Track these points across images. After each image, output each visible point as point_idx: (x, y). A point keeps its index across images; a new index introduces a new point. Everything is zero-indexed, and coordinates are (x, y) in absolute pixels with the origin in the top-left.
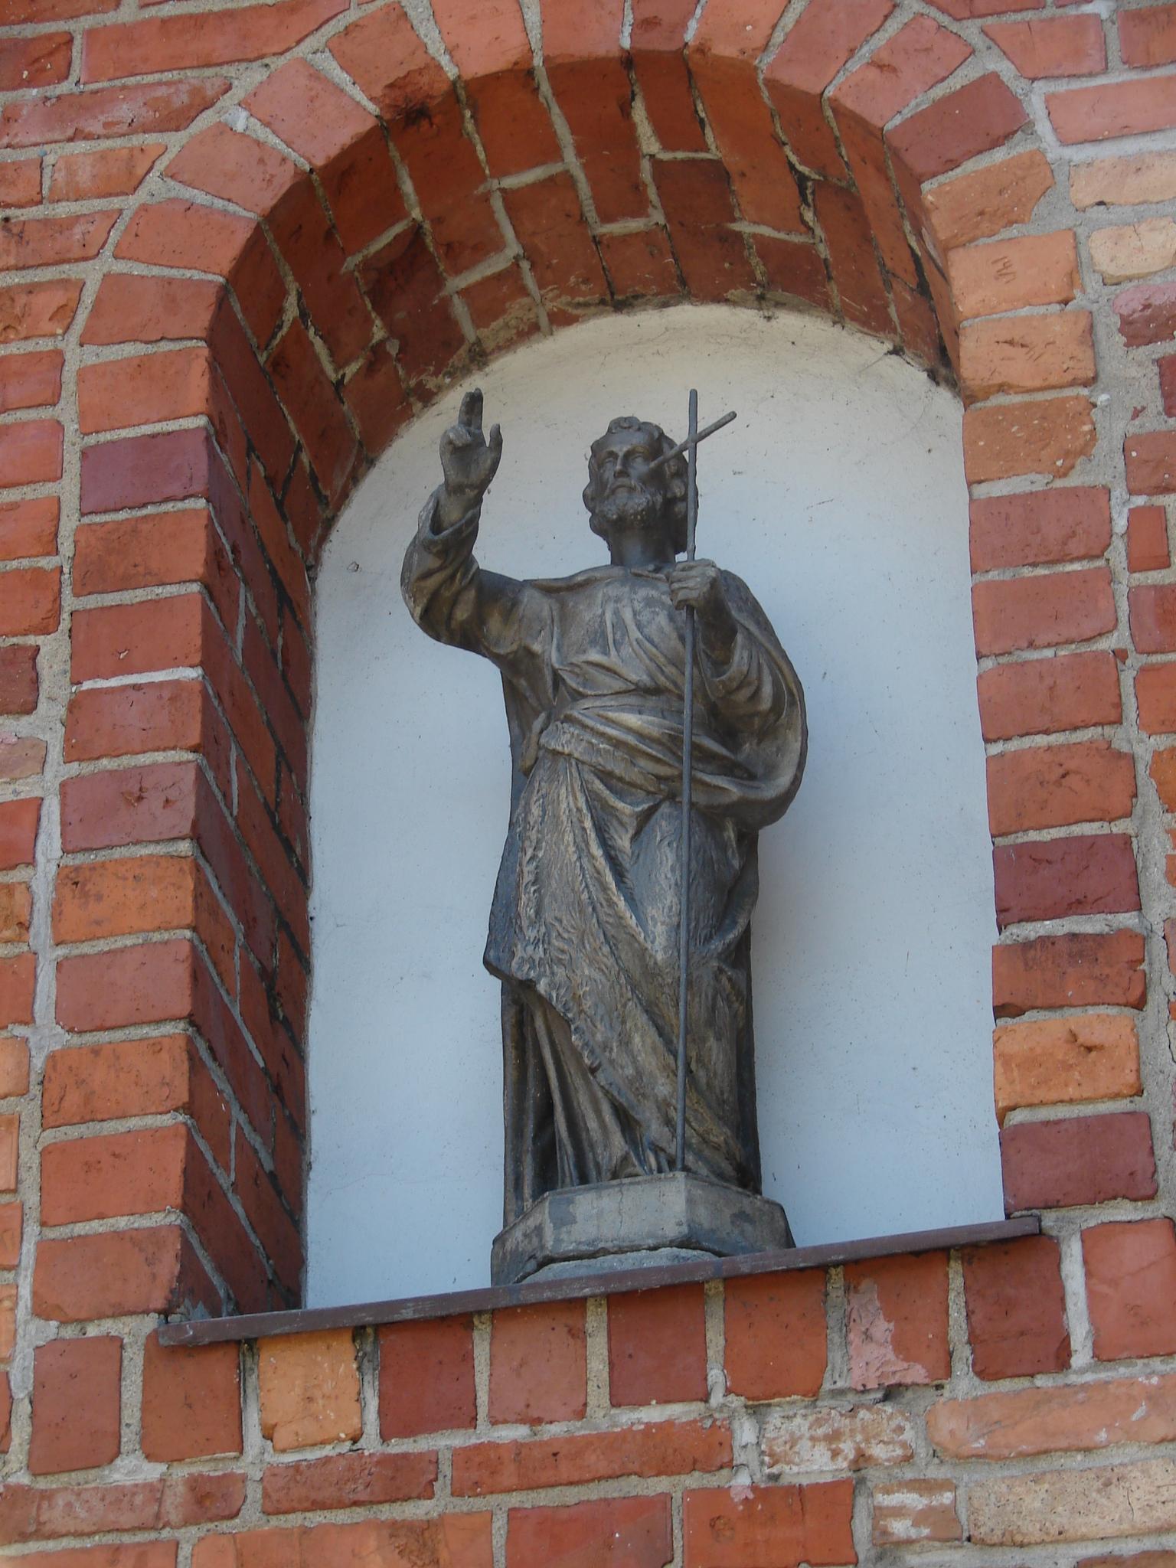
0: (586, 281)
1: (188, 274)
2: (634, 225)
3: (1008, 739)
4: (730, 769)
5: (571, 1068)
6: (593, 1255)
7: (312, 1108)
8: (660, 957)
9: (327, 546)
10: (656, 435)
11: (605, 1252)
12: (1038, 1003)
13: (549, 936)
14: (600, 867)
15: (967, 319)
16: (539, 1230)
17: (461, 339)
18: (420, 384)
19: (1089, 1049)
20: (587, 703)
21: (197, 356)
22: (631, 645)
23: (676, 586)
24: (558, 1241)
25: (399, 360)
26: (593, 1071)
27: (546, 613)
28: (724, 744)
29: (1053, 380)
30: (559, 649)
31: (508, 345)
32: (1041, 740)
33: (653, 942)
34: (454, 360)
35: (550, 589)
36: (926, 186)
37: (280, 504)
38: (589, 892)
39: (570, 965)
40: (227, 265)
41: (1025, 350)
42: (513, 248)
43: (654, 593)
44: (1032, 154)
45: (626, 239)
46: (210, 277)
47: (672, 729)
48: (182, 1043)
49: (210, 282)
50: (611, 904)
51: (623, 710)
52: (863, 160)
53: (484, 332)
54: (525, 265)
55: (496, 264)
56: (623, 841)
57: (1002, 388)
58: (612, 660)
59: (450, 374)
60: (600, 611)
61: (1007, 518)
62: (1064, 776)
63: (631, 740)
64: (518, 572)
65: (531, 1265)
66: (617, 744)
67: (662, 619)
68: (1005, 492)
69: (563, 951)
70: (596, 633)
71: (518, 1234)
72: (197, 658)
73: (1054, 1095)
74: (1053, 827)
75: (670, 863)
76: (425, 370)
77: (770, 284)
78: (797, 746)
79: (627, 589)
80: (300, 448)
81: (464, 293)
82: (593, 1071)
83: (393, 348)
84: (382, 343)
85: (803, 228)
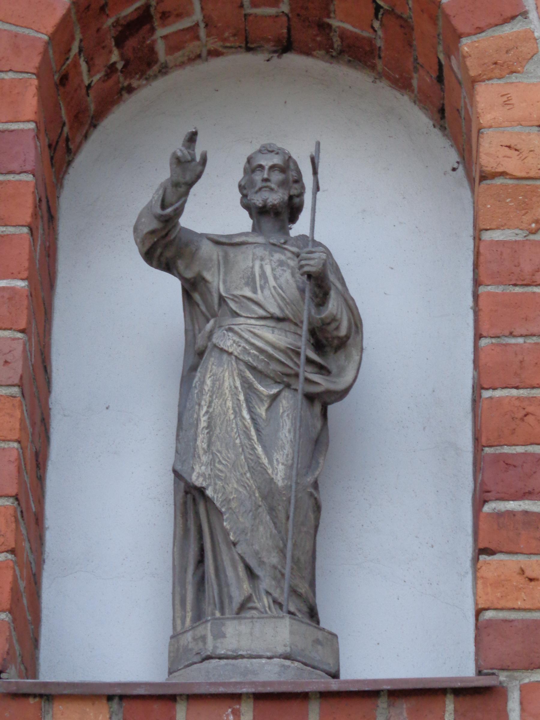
0: (234, 35)
1: (27, 31)
2: (271, 11)
3: (495, 389)
4: (322, 369)
5: (220, 538)
6: (235, 658)
7: (47, 526)
8: (280, 484)
9: (67, 176)
10: (287, 158)
11: (242, 657)
12: (504, 550)
13: (214, 461)
14: (248, 426)
15: (484, 128)
16: (203, 638)
17: (156, 61)
18: (130, 85)
19: (531, 580)
20: (241, 320)
21: (31, 85)
22: (270, 289)
23: (303, 262)
24: (215, 647)
25: (122, 72)
26: (235, 544)
27: (215, 257)
28: (318, 355)
29: (532, 174)
30: (225, 282)
31: (182, 65)
32: (514, 392)
33: (277, 474)
34: (150, 72)
35: (217, 242)
36: (465, 41)
37: (52, 158)
38: (240, 439)
39: (225, 480)
40: (50, 30)
41: (517, 153)
42: (198, 16)
43: (283, 257)
44: (526, 31)
45: (263, 17)
46: (40, 35)
47: (290, 344)
48: (11, 511)
49: (40, 38)
50: (254, 449)
51: (265, 329)
52: (422, 11)
53: (170, 58)
54: (202, 25)
55: (185, 23)
56: (262, 410)
57: (503, 174)
58: (259, 297)
59: (146, 79)
60: (251, 265)
61: (502, 253)
62: (526, 415)
63: (270, 350)
64: (199, 229)
65: (197, 659)
66: (261, 351)
67: (287, 275)
68: (501, 238)
69: (221, 471)
70: (248, 278)
71: (189, 636)
72: (25, 274)
73: (510, 605)
74: (518, 445)
75: (287, 428)
76: (134, 77)
77: (341, 52)
78: (357, 358)
79: (267, 253)
80: (64, 124)
81: (165, 37)
82: (235, 544)
83: (120, 66)
84: (115, 63)
85: (371, 30)
